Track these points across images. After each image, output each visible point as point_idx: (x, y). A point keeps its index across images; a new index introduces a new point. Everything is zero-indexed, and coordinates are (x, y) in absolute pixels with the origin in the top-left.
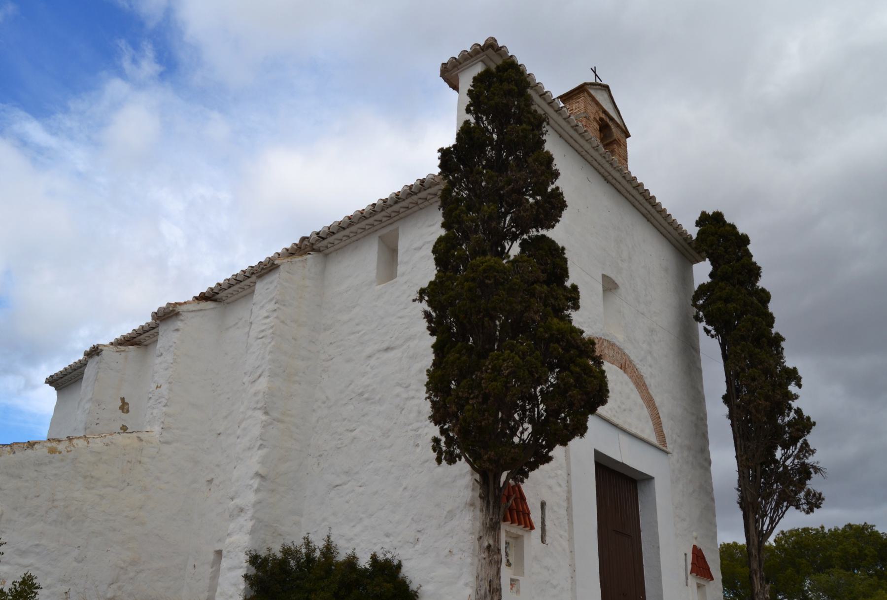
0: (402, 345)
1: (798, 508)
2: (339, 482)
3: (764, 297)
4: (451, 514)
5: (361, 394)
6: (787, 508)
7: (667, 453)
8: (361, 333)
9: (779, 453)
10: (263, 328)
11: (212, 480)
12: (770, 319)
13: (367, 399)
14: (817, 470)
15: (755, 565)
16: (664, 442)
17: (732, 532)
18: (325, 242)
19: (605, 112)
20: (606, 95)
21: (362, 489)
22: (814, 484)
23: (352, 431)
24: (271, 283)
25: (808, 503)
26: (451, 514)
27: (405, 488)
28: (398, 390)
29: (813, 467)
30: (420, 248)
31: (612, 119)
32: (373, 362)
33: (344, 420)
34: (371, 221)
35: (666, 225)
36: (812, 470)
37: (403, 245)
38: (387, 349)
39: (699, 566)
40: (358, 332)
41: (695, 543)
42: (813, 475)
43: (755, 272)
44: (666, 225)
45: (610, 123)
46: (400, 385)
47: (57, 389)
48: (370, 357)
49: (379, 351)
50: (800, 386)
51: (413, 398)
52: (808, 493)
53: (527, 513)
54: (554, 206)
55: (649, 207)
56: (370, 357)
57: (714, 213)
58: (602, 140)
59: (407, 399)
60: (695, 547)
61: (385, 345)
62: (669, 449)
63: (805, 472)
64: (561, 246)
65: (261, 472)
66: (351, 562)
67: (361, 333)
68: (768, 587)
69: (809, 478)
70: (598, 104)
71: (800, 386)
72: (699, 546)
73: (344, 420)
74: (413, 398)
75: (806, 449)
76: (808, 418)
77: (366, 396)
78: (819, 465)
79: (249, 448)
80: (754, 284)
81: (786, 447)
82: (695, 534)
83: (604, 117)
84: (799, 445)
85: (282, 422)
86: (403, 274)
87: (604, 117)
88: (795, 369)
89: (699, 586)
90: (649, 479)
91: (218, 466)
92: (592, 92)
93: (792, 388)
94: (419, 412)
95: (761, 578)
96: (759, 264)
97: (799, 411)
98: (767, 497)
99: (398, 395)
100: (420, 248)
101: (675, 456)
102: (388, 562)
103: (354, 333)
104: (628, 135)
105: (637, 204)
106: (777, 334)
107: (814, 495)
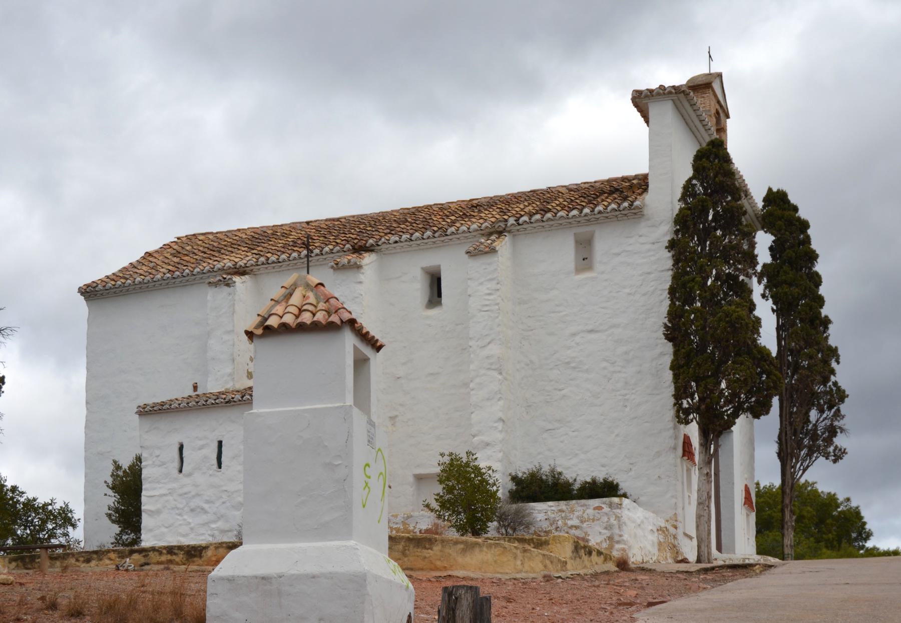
0: (606, 330)
1: (827, 459)
2: (550, 426)
3: (817, 280)
4: (658, 454)
5: (568, 363)
6: (817, 458)
8: (562, 314)
9: (813, 414)
11: (396, 416)
12: (821, 301)
13: (574, 368)
14: (842, 430)
15: (787, 501)
17: (770, 475)
21: (576, 433)
22: (840, 441)
23: (560, 390)
24: (489, 264)
25: (835, 455)
26: (658, 454)
27: (617, 435)
28: (605, 364)
29: (840, 428)
30: (619, 254)
32: (577, 339)
33: (551, 381)
36: (838, 430)
38: (591, 331)
40: (559, 312)
42: (839, 434)
43: (812, 257)
46: (607, 361)
47: (87, 299)
48: (574, 335)
49: (583, 331)
50: (838, 363)
51: (620, 372)
52: (836, 447)
53: (693, 455)
56: (574, 335)
57: (778, 190)
59: (614, 372)
60: (746, 486)
61: (590, 327)
63: (832, 431)
64: (834, 346)
65: (503, 418)
67: (562, 314)
68: (794, 517)
69: (835, 436)
71: (838, 363)
73: (551, 381)
74: (620, 372)
75: (838, 414)
76: (844, 391)
77: (573, 365)
78: (844, 427)
79: (488, 399)
80: (810, 269)
81: (822, 411)
84: (833, 410)
88: (836, 348)
91: (401, 405)
93: (834, 364)
94: (626, 383)
95: (791, 511)
96: (817, 252)
97: (835, 384)
98: (800, 447)
99: (605, 368)
100: (619, 254)
102: (612, 483)
103: (554, 312)
104: (728, 116)
106: (826, 317)
107: (840, 450)
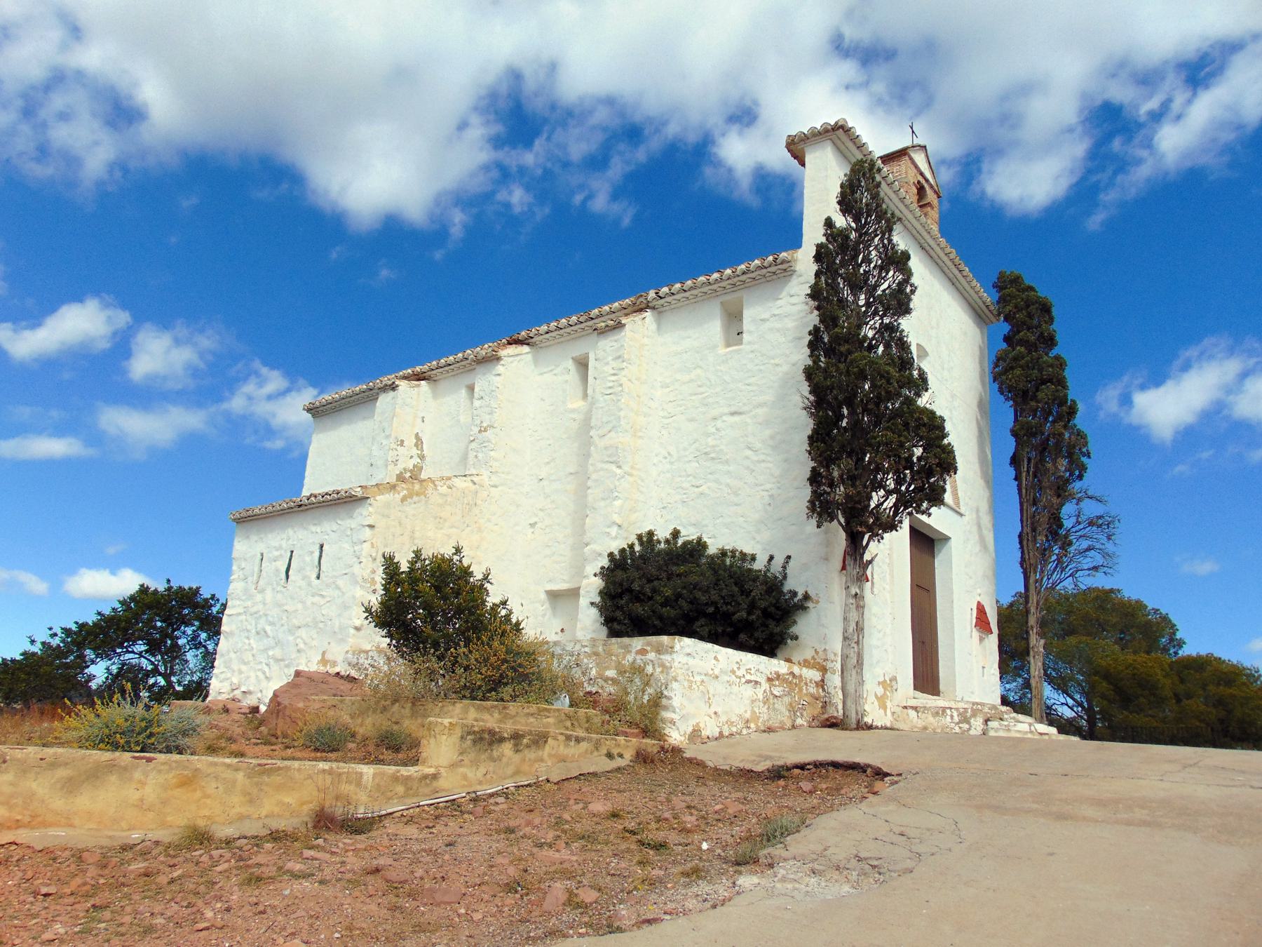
7: (961, 515)
10: (611, 384)
16: (958, 504)
18: (662, 301)
19: (922, 174)
20: (923, 155)
28: (748, 453)
31: (927, 181)
32: (719, 423)
34: (715, 287)
35: (968, 288)
37: (748, 314)
39: (982, 622)
41: (979, 599)
44: (968, 288)
45: (926, 185)
54: (900, 302)
55: (956, 272)
58: (919, 201)
59: (759, 462)
61: (733, 409)
62: (962, 510)
66: (13, 661)
68: (1042, 642)
70: (916, 167)
72: (983, 603)
77: (713, 455)
82: (979, 591)
83: (923, 181)
85: (631, 475)
86: (749, 343)
87: (923, 181)
89: (981, 639)
90: (946, 539)
92: (913, 155)
101: (969, 517)
105: (945, 269)
